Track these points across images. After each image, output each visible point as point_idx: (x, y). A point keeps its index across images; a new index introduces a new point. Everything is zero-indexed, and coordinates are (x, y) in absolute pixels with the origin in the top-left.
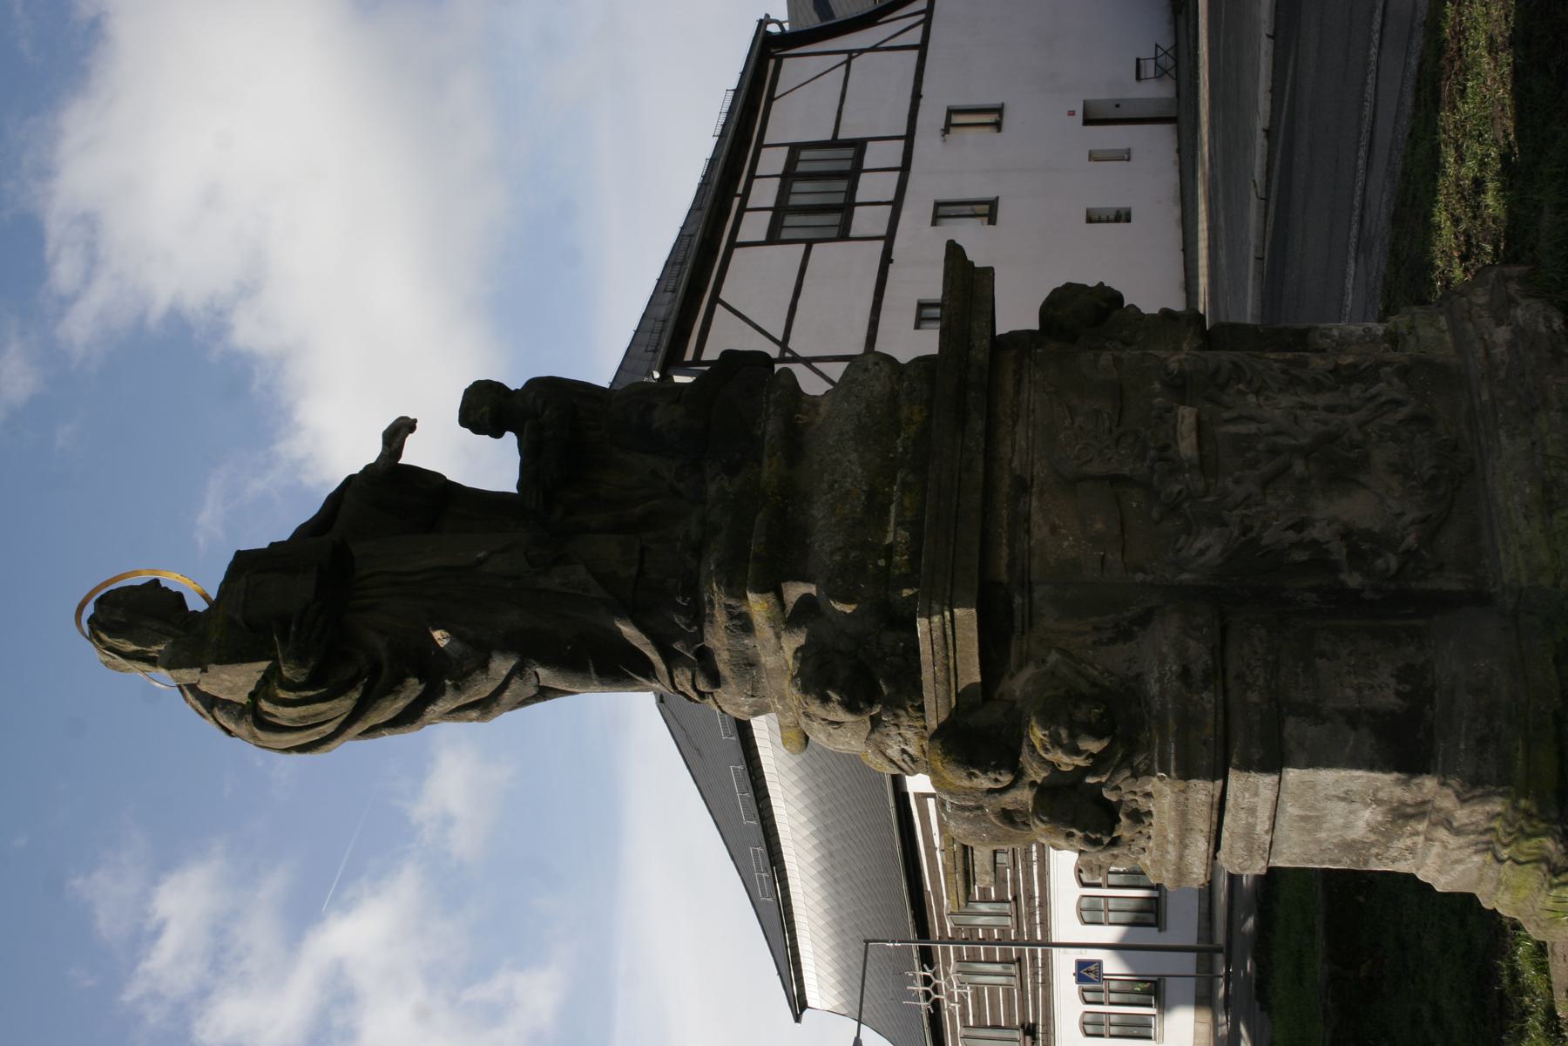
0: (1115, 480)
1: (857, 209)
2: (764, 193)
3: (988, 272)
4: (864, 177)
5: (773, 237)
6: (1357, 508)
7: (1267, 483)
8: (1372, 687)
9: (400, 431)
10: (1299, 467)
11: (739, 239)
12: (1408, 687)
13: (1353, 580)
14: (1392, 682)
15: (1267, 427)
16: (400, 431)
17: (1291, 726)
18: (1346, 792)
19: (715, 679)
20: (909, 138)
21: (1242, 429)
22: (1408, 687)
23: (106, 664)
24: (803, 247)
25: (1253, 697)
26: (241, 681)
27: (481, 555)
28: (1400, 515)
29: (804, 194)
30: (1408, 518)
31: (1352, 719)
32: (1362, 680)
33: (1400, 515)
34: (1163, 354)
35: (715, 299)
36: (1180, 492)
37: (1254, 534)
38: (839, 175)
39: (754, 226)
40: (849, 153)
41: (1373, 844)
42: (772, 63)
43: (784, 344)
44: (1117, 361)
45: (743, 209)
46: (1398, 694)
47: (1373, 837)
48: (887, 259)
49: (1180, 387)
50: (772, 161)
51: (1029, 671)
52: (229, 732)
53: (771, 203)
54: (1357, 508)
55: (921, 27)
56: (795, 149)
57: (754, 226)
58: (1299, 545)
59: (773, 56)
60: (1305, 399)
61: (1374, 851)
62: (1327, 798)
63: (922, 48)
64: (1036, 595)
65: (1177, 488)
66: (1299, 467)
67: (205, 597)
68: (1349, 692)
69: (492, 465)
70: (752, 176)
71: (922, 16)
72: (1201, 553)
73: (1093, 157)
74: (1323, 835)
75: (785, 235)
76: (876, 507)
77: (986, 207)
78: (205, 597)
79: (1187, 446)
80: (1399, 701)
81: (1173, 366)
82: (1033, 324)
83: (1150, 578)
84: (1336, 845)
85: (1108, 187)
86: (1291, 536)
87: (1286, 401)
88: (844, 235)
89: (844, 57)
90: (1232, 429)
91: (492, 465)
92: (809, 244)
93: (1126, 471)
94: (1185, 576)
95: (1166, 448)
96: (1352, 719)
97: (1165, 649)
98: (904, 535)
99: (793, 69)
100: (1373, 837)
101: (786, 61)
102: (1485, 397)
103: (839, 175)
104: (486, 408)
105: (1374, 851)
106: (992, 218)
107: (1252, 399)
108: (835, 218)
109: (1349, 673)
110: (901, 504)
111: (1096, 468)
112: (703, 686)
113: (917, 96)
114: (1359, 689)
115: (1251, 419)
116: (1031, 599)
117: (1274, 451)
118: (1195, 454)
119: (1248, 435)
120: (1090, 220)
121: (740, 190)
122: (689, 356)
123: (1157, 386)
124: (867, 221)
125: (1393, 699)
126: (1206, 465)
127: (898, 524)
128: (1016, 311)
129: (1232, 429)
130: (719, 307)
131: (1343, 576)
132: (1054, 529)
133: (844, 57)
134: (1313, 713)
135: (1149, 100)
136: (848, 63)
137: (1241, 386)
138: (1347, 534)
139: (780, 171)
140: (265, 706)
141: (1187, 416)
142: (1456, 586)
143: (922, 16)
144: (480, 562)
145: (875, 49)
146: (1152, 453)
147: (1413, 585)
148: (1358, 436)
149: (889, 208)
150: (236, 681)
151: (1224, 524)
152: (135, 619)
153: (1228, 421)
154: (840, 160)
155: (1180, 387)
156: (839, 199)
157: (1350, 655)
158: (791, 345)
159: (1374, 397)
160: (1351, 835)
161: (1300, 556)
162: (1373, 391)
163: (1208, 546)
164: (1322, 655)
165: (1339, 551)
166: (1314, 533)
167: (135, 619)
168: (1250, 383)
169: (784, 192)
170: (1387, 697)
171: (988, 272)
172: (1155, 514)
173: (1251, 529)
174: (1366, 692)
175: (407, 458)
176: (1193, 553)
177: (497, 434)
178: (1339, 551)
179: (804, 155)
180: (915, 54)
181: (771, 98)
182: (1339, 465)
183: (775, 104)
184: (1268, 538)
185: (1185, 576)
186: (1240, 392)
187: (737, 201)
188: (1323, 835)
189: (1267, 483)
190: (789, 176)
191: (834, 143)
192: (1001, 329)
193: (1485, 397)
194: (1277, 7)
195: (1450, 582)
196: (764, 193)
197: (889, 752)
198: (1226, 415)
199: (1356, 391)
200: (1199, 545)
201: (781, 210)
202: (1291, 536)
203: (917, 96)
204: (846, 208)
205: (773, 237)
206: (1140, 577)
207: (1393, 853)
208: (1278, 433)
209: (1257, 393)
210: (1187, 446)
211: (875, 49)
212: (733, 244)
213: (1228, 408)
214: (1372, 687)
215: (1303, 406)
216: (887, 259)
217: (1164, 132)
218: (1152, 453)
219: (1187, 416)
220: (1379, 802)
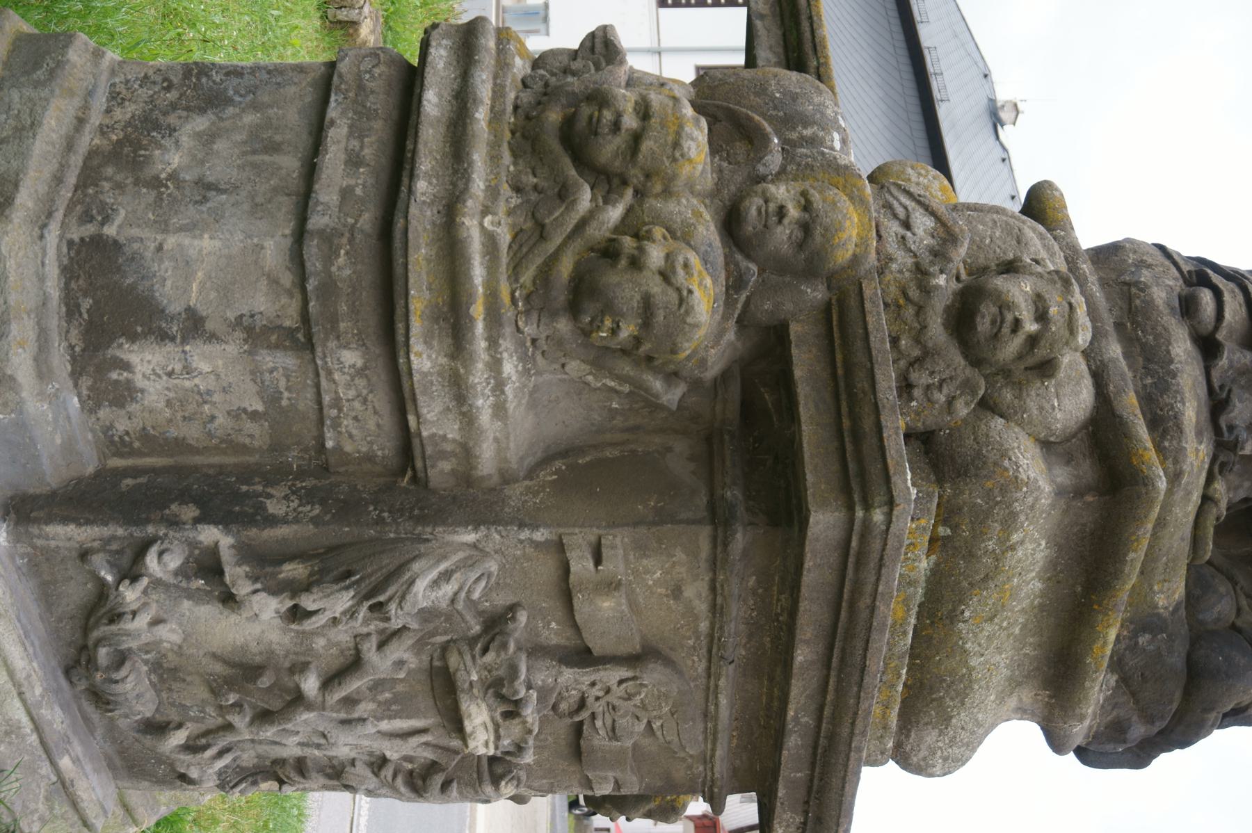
3: (698, 68)
8: (170, 374)
10: (310, 685)
12: (114, 376)
13: (210, 534)
14: (140, 382)
18: (205, 199)
22: (114, 376)
28: (156, 622)
30: (142, 621)
32: (187, 384)
33: (156, 622)
36: (485, 650)
37: (367, 604)
41: (174, 106)
46: (127, 366)
47: (172, 119)
61: (172, 95)
62: (236, 188)
64: (702, 500)
68: (205, 367)
72: (446, 576)
74: (250, 118)
80: (125, 356)
83: (525, 534)
84: (229, 101)
86: (308, 602)
100: (172, 119)
105: (172, 95)
109: (209, 392)
111: (612, 675)
114: (188, 370)
116: (712, 494)
118: (464, 706)
119: (390, 718)
125: (134, 359)
137: (410, 766)
147: (120, 532)
153: (424, 731)
157: (213, 418)
159: (220, 754)
160: (201, 123)
161: (293, 570)
162: (227, 760)
164: (254, 416)
170: (145, 362)
171: (698, 68)
174: (178, 367)
178: (236, 575)
184: (342, 601)
185: (470, 537)
188: (250, 118)
194: (472, 826)
195: (65, 535)
197: (930, 223)
213: (426, 744)
214: (170, 374)
215: (318, 746)
220: (156, 183)
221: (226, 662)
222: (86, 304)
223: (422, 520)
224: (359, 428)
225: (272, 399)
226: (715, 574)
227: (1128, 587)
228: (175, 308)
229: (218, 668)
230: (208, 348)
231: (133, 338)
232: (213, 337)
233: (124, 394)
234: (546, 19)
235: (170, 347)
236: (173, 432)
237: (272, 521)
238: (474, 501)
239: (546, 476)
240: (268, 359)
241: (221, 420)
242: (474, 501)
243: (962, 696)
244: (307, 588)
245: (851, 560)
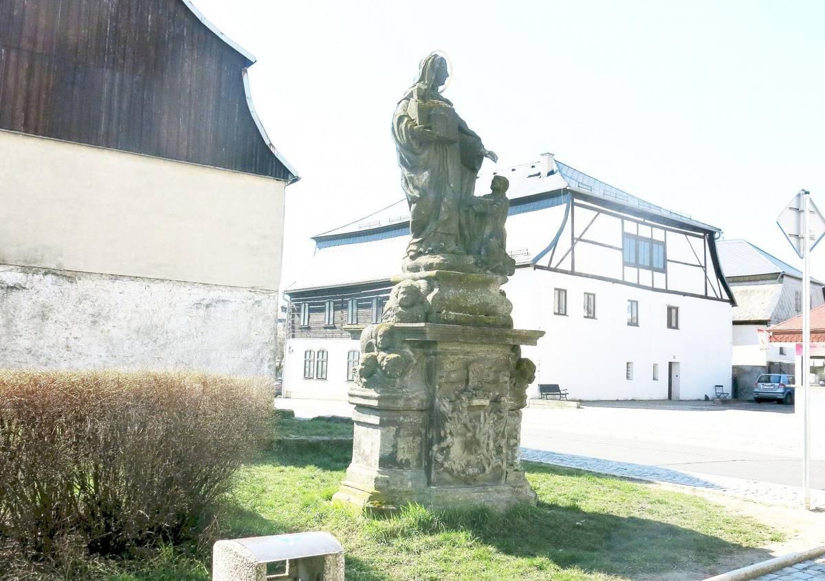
0: (467, 381)
1: (636, 269)
2: (645, 231)
4: (650, 272)
5: (626, 235)
6: (456, 450)
7: (465, 425)
9: (493, 157)
10: (469, 434)
11: (625, 221)
13: (435, 448)
15: (482, 426)
16: (493, 157)
17: (393, 429)
19: (413, 258)
20: (666, 291)
21: (482, 419)
22: (403, 462)
23: (421, 61)
24: (621, 247)
25: (401, 418)
26: (413, 111)
27: (452, 185)
29: (645, 247)
31: (395, 446)
34: (508, 396)
35: (600, 211)
37: (449, 420)
38: (651, 262)
39: (631, 227)
40: (661, 266)
42: (702, 234)
43: (580, 239)
44: (506, 382)
45: (638, 222)
48: (615, 281)
49: (496, 401)
50: (658, 234)
51: (411, 353)
52: (399, 103)
53: (640, 234)
54: (456, 450)
55: (715, 297)
56: (664, 244)
57: (631, 227)
58: (446, 433)
59: (705, 234)
60: (491, 438)
63: (706, 297)
64: (433, 357)
65: (464, 398)
66: (469, 434)
67: (442, 92)
69: (482, 187)
70: (652, 226)
71: (720, 297)
72: (444, 405)
73: (655, 366)
75: (627, 240)
76: (459, 309)
77: (635, 322)
78: (442, 92)
79: (476, 402)
81: (503, 399)
82: (523, 356)
85: (642, 371)
86: (448, 431)
87: (491, 432)
88: (625, 264)
89: (703, 265)
90: (482, 416)
91: (482, 187)
92: (622, 250)
93: (470, 384)
94: (437, 400)
95: (476, 396)
96: (395, 446)
97: (416, 393)
98: (452, 318)
99: (699, 244)
101: (703, 240)
102: (490, 489)
103: (651, 262)
104: (500, 184)
106: (631, 324)
107: (492, 421)
108: (633, 261)
110: (462, 316)
112: (412, 253)
113: (685, 294)
115: (485, 421)
117: (474, 427)
120: (628, 363)
121: (646, 221)
122: (576, 201)
123: (497, 394)
124: (631, 274)
126: (471, 408)
127: (456, 315)
128: (526, 352)
129: (482, 416)
130: (596, 213)
131: (436, 445)
132: (453, 362)
133: (703, 265)
134: (397, 435)
135: (679, 389)
136: (701, 266)
138: (448, 447)
139: (654, 238)
140: (406, 119)
141: (486, 402)
142: (432, 477)
143: (720, 297)
144: (449, 185)
145: (706, 277)
146: (474, 392)
148: (479, 452)
149: (636, 282)
150: (413, 112)
151: (452, 412)
152: (435, 71)
153: (485, 416)
154: (658, 263)
155: (496, 401)
156: (641, 262)
158: (579, 242)
159: (492, 458)
161: (442, 434)
162: (493, 457)
163: (446, 407)
164: (414, 438)
165: (444, 444)
166: (449, 437)
167: (435, 71)
168: (497, 421)
169: (646, 240)
170: (401, 456)
172: (456, 392)
173: (451, 420)
175: (485, 159)
176: (444, 403)
177: (492, 188)
178: (444, 444)
179: (661, 247)
180: (704, 294)
181: (686, 234)
182: (471, 445)
183: (684, 236)
185: (437, 400)
186: (494, 418)
187: (642, 220)
189: (465, 425)
190: (651, 241)
191: (665, 260)
192: (521, 346)
193: (490, 489)
196: (645, 231)
198: (487, 414)
199: (494, 452)
200: (447, 405)
201: (637, 238)
202: (448, 431)
203: (685, 294)
204: (637, 265)
205: (626, 235)
206: (437, 387)
207: (357, 456)
208: (480, 429)
209: (494, 423)
210: (476, 402)
211: (706, 277)
212: (623, 218)
213: (489, 415)
215: (489, 437)
216: (615, 281)
217: (664, 394)
218: (474, 392)
219: (486, 402)
221: (465, 451)
222: (390, 465)
223: (433, 408)
224: (416, 419)
225: (410, 435)
226: (425, 410)
227: (446, 347)
228: (391, 450)
229: (465, 453)
230: (399, 443)
231: (396, 457)
232: (397, 443)
233: (407, 461)
234: (559, 314)
235: (399, 451)
236: (417, 454)
237: (433, 437)
238: (431, 398)
239: (429, 386)
240: (401, 434)
241: (414, 445)
242: (431, 398)
243: (487, 304)
244: (445, 431)
245: (807, 402)
